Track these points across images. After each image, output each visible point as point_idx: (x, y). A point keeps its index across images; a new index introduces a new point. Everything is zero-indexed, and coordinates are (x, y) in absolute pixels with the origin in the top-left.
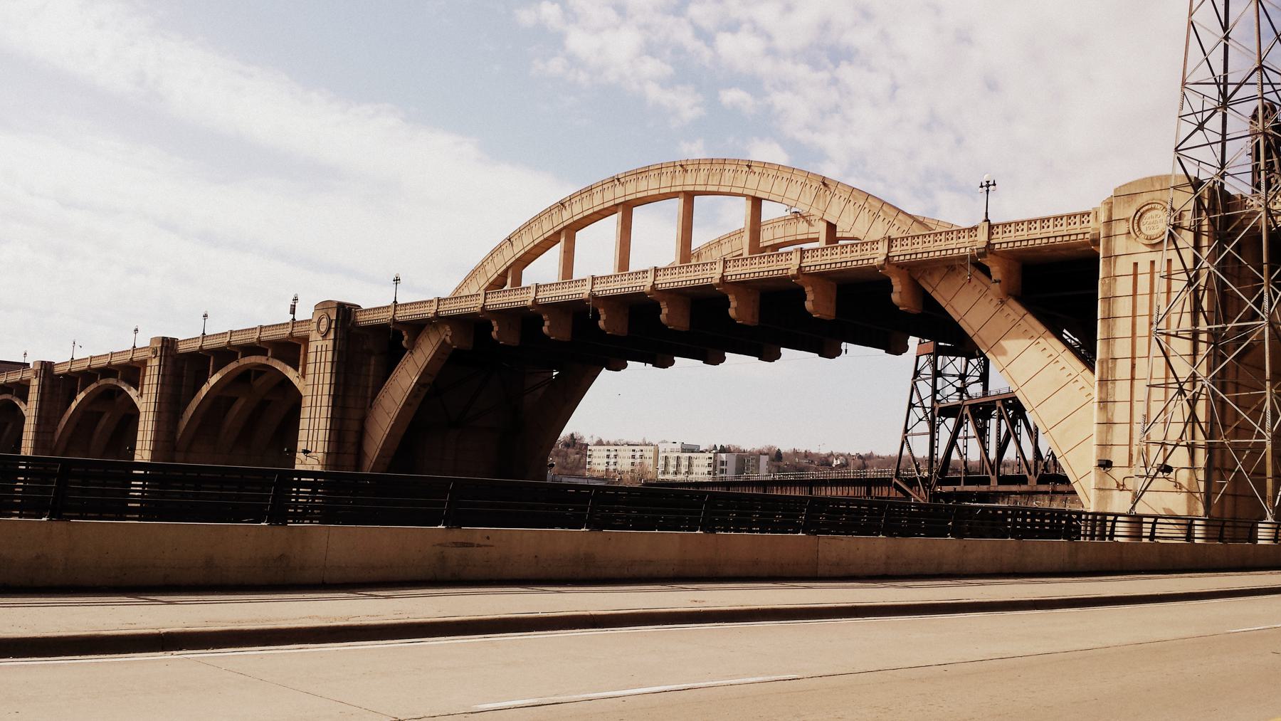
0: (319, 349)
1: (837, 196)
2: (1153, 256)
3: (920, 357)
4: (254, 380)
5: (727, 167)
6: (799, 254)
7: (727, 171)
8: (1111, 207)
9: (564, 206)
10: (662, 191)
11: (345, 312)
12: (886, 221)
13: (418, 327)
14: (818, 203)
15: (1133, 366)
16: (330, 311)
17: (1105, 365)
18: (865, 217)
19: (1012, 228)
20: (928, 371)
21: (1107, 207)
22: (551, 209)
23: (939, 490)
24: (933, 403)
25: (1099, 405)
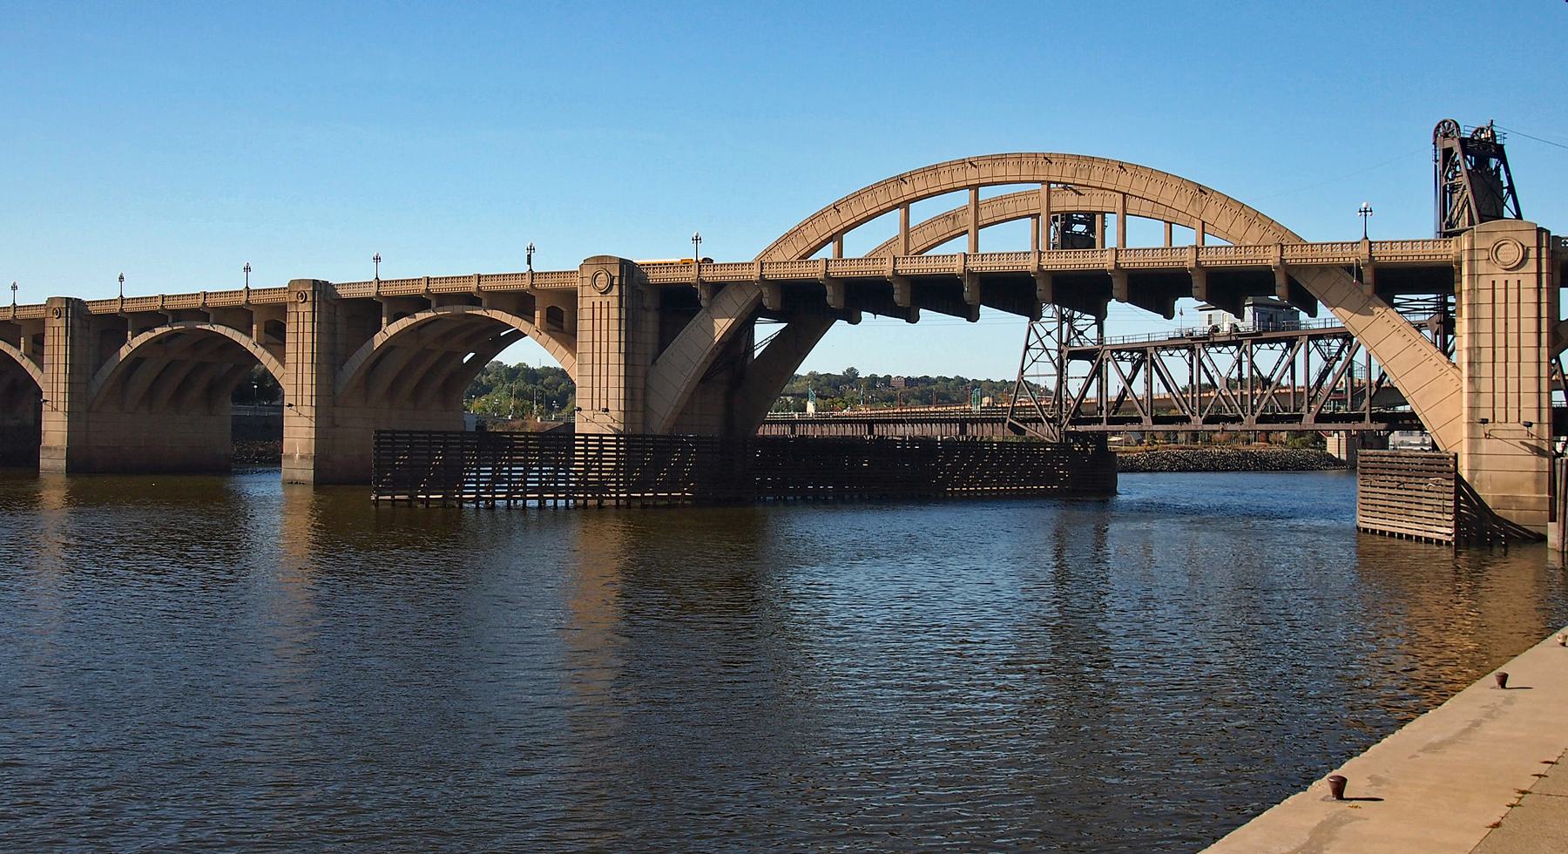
1: (1213, 202)
4: (132, 338)
6: (1194, 250)
7: (1096, 168)
11: (628, 269)
13: (717, 288)
14: (1194, 205)
15: (1494, 353)
17: (1472, 352)
18: (1241, 221)
19: (726, 267)
22: (886, 182)
23: (1073, 429)
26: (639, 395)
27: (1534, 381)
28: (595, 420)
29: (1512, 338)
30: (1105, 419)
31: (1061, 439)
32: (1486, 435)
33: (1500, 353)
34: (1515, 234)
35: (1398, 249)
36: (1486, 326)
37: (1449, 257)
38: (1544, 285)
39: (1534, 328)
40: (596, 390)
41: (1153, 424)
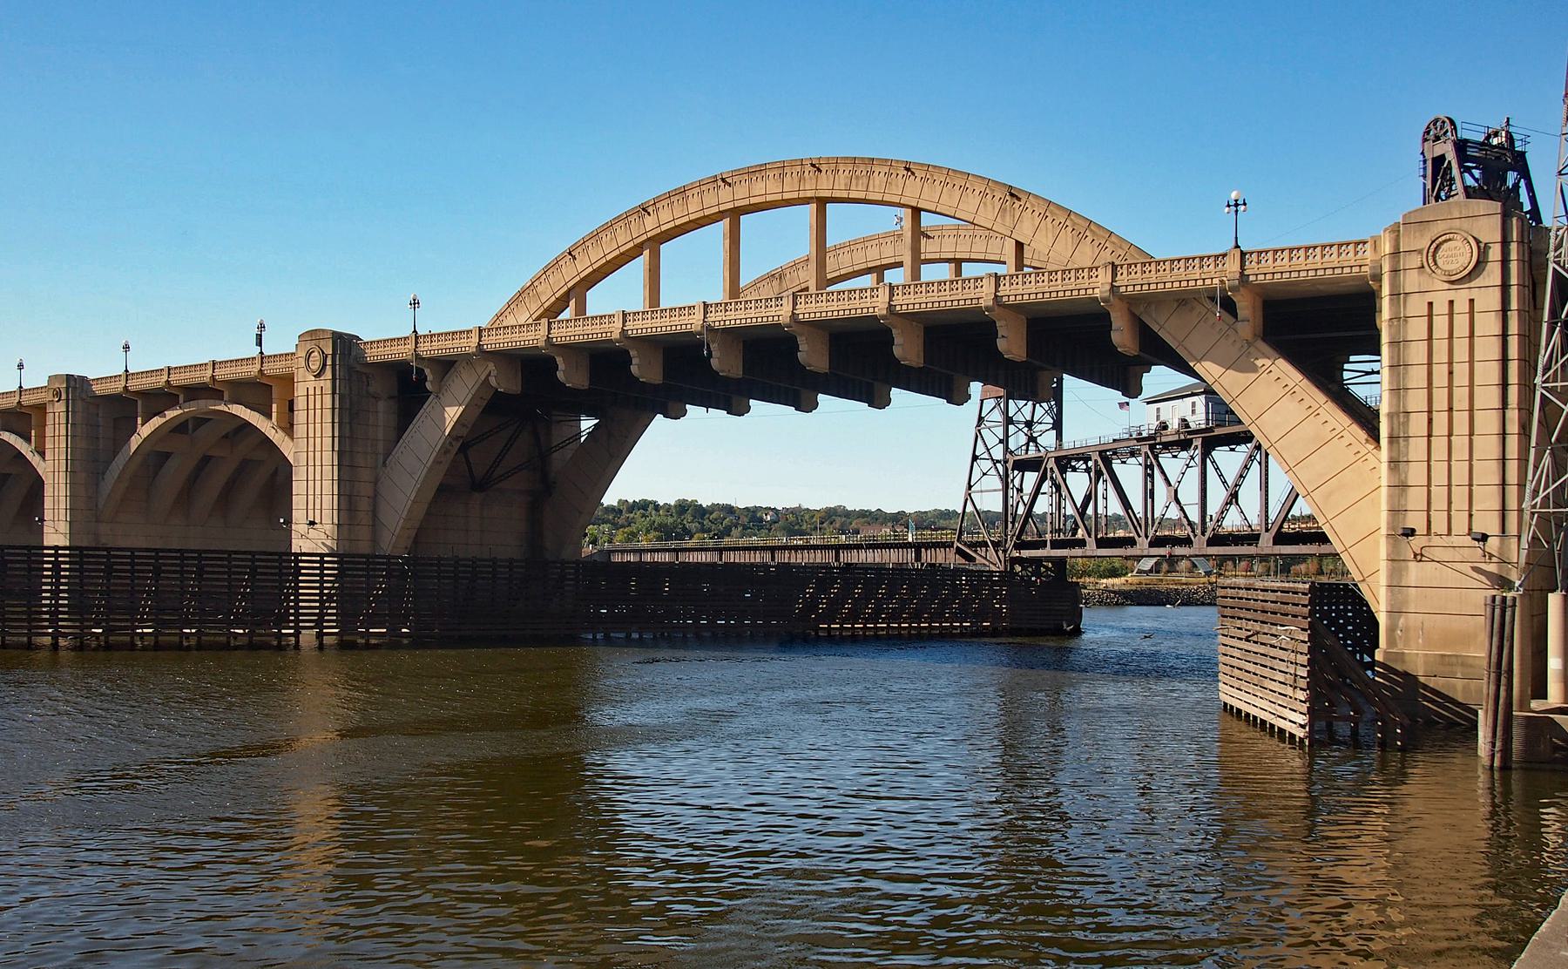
0: (311, 392)
1: (1030, 211)
2: (1451, 295)
3: (985, 401)
4: (194, 430)
5: (877, 169)
6: (993, 280)
7: (876, 174)
8: (1398, 236)
9: (646, 211)
10: (786, 196)
11: (345, 345)
12: (1096, 243)
13: (446, 365)
14: (1003, 217)
15: (1430, 421)
16: (322, 343)
18: (1067, 238)
20: (997, 416)
21: (1393, 235)
22: (628, 215)
23: (1018, 555)
24: (1005, 455)
25: (1389, 466)
26: (364, 505)
27: (1494, 466)
28: (310, 536)
29: (1461, 395)
30: (1048, 542)
31: (1006, 568)
32: (1415, 555)
33: (1440, 420)
34: (1466, 224)
35: (1284, 263)
36: (1417, 377)
37: (1363, 269)
38: (1514, 305)
39: (1495, 378)
40: (311, 498)
41: (1097, 548)
